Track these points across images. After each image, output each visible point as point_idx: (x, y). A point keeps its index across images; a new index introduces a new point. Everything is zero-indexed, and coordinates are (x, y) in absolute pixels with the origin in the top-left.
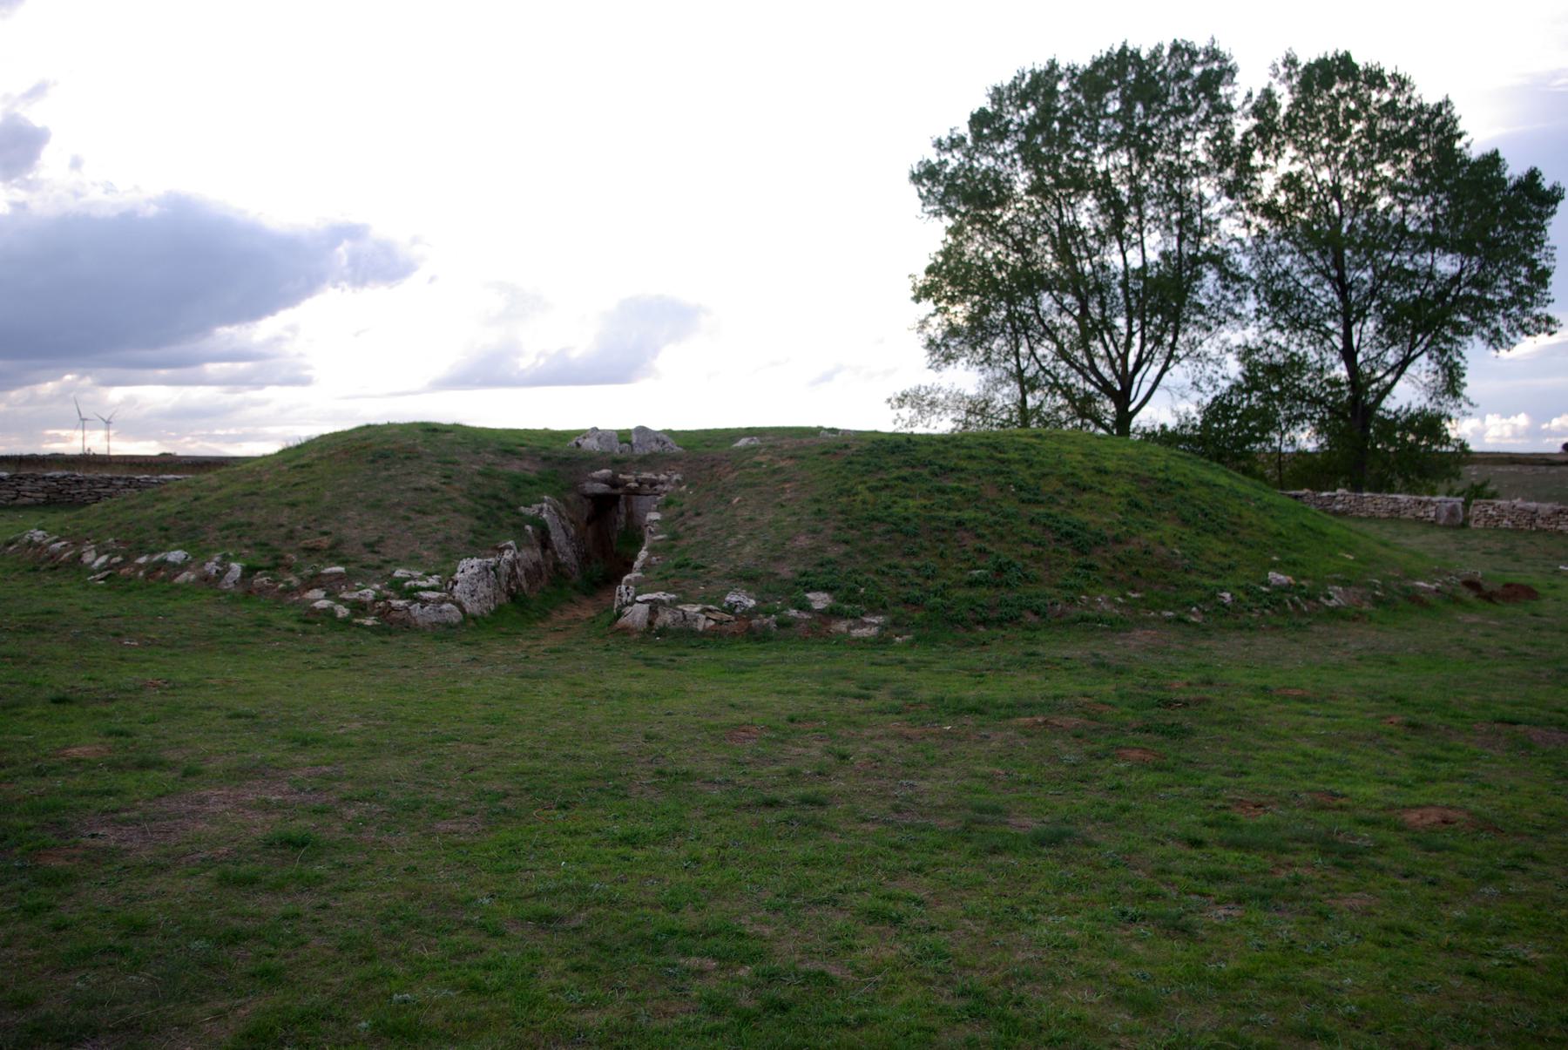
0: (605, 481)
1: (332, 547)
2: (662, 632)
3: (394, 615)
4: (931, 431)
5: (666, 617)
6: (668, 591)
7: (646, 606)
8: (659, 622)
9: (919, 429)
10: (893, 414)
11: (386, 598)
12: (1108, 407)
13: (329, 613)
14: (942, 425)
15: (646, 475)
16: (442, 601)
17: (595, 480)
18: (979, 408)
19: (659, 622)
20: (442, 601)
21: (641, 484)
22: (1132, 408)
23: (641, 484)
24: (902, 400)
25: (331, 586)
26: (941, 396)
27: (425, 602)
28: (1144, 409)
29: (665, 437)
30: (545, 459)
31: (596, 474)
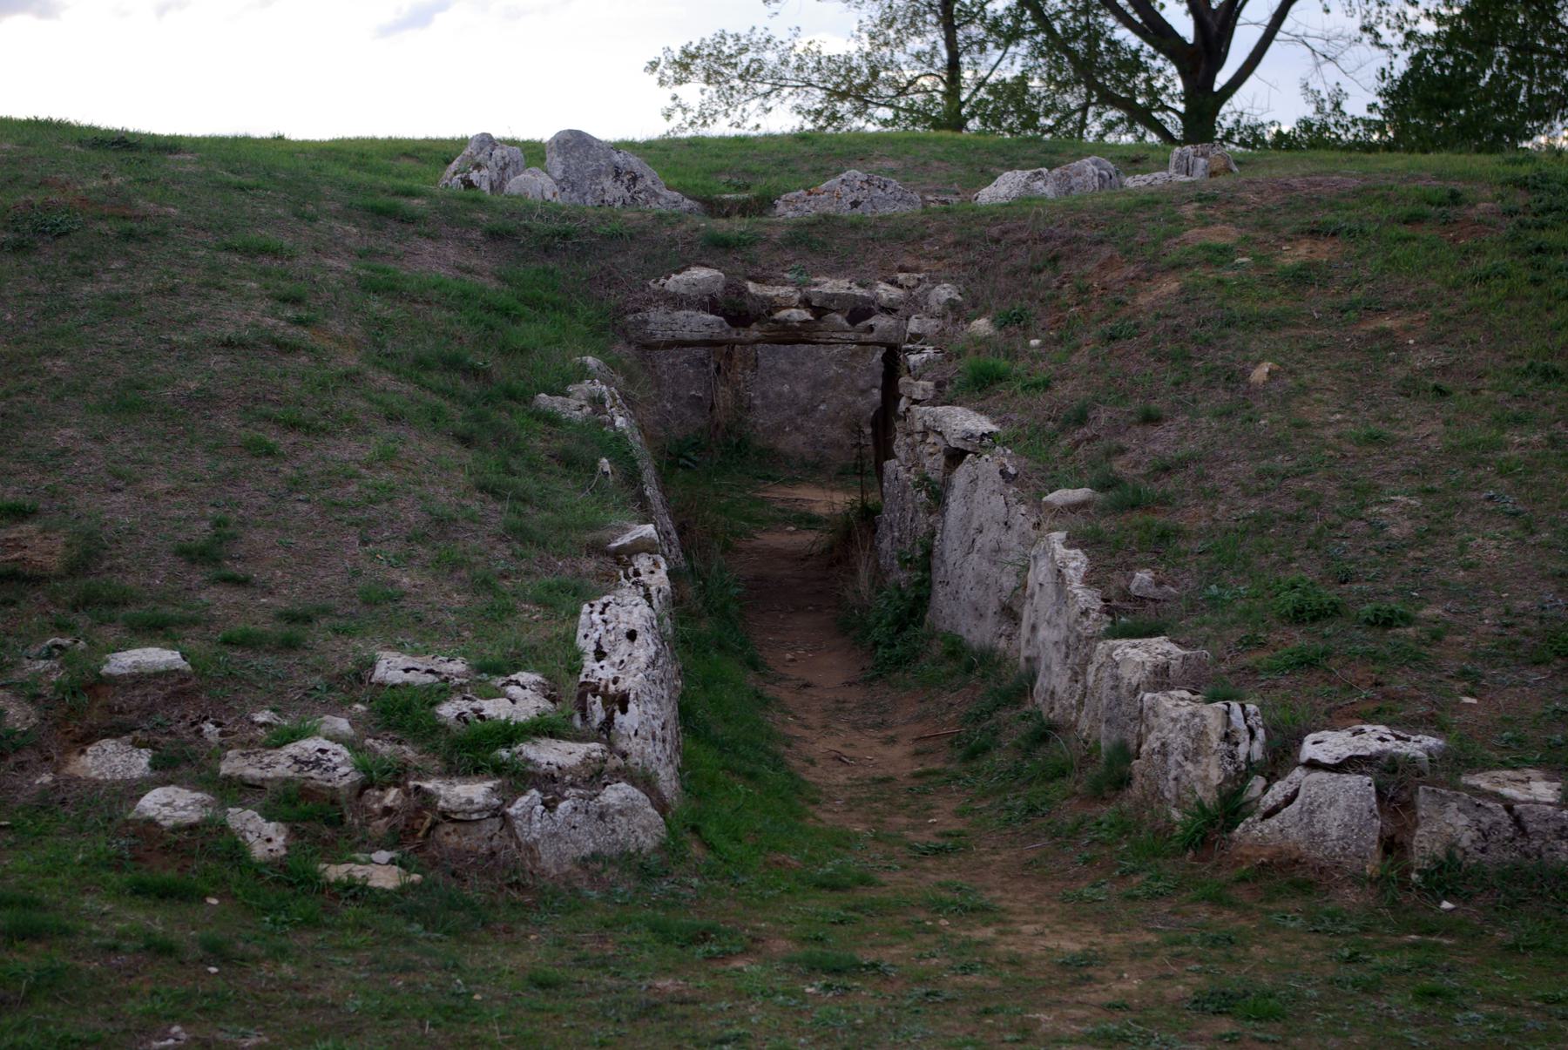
0: (711, 304)
1: (75, 569)
2: (1448, 875)
3: (450, 838)
4: (747, 130)
5: (1444, 825)
6: (1409, 725)
7: (1359, 785)
8: (1426, 842)
9: (720, 128)
10: (663, 97)
11: (397, 774)
12: (1169, 78)
13: (208, 844)
14: (781, 118)
15: (832, 285)
16: (595, 776)
17: (676, 301)
18: (852, 85)
19: (1426, 842)
20: (595, 776)
21: (819, 312)
22: (1222, 78)
23: (819, 312)
24: (684, 64)
25: (171, 725)
26: (771, 57)
27: (550, 783)
28: (1251, 81)
29: (635, 163)
30: (496, 235)
31: (676, 282)
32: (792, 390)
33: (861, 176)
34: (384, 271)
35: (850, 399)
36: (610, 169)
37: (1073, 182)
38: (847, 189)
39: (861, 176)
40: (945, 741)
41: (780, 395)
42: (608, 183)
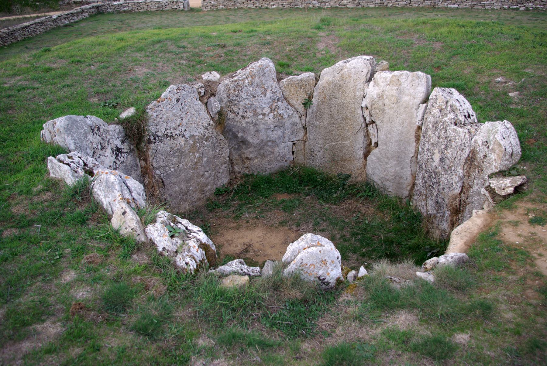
32: (179, 188)
33: (175, 87)
34: (103, 44)
35: (199, 181)
36: (89, 130)
37: (265, 71)
38: (172, 95)
39: (175, 87)
40: (135, 27)
41: (176, 192)
42: (91, 137)
